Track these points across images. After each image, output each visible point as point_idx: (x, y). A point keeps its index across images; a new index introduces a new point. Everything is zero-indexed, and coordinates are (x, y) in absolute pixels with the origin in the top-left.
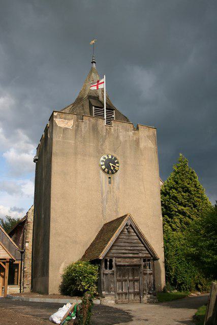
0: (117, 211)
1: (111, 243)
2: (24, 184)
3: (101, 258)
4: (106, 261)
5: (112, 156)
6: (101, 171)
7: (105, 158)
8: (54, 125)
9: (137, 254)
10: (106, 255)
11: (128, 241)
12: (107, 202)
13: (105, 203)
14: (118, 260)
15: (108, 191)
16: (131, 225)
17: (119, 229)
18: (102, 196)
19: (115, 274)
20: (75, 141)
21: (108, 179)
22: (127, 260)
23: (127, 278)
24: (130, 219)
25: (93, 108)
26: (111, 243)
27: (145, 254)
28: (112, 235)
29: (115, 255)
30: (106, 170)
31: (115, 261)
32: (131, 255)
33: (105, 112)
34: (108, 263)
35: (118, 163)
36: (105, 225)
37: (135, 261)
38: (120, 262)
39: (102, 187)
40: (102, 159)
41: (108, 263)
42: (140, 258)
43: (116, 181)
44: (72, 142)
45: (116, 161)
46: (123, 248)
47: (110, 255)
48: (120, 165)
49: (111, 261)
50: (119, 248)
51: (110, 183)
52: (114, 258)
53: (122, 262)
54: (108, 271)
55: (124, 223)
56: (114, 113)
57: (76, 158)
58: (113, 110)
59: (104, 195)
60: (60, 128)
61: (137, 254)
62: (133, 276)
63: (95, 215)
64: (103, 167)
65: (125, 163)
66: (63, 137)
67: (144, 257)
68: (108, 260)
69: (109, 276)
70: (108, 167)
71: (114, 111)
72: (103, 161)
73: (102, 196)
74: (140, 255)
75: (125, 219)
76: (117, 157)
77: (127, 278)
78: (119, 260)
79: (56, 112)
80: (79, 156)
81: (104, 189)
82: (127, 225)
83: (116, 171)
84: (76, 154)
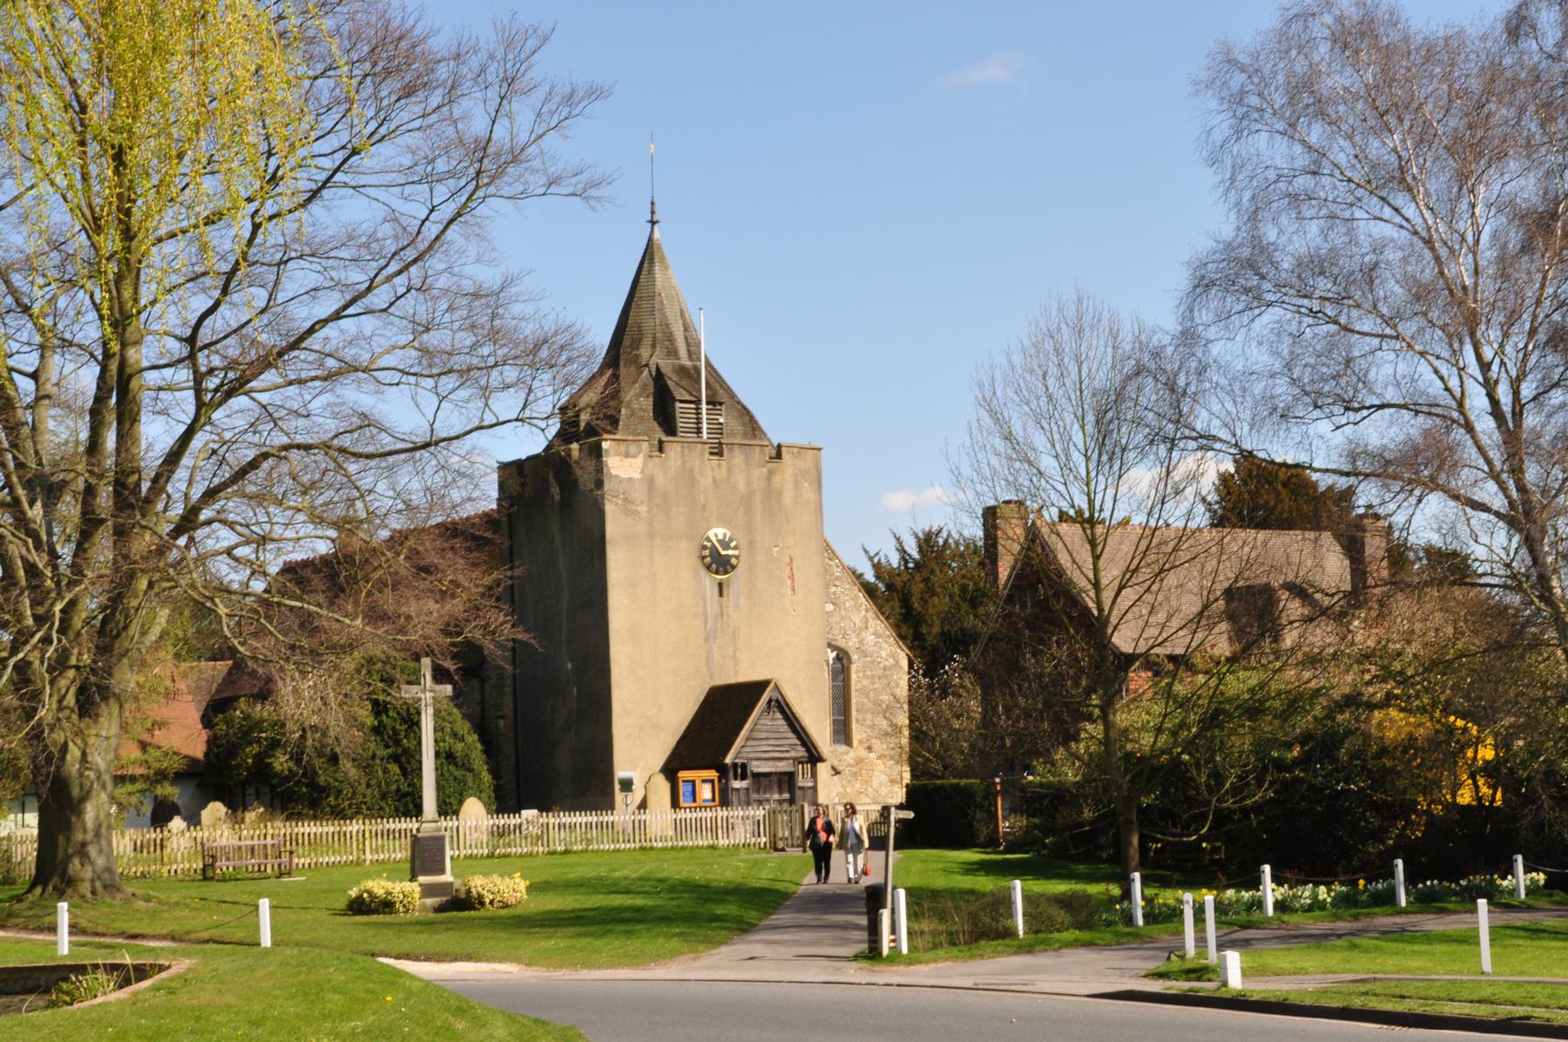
12: (715, 637)
14: (754, 763)
16: (777, 701)
22: (770, 763)
25: (678, 405)
33: (704, 411)
39: (705, 607)
46: (764, 742)
49: (744, 766)
51: (721, 594)
59: (710, 623)
74: (793, 754)
80: (658, 541)
82: (770, 701)
83: (734, 567)
84: (651, 536)
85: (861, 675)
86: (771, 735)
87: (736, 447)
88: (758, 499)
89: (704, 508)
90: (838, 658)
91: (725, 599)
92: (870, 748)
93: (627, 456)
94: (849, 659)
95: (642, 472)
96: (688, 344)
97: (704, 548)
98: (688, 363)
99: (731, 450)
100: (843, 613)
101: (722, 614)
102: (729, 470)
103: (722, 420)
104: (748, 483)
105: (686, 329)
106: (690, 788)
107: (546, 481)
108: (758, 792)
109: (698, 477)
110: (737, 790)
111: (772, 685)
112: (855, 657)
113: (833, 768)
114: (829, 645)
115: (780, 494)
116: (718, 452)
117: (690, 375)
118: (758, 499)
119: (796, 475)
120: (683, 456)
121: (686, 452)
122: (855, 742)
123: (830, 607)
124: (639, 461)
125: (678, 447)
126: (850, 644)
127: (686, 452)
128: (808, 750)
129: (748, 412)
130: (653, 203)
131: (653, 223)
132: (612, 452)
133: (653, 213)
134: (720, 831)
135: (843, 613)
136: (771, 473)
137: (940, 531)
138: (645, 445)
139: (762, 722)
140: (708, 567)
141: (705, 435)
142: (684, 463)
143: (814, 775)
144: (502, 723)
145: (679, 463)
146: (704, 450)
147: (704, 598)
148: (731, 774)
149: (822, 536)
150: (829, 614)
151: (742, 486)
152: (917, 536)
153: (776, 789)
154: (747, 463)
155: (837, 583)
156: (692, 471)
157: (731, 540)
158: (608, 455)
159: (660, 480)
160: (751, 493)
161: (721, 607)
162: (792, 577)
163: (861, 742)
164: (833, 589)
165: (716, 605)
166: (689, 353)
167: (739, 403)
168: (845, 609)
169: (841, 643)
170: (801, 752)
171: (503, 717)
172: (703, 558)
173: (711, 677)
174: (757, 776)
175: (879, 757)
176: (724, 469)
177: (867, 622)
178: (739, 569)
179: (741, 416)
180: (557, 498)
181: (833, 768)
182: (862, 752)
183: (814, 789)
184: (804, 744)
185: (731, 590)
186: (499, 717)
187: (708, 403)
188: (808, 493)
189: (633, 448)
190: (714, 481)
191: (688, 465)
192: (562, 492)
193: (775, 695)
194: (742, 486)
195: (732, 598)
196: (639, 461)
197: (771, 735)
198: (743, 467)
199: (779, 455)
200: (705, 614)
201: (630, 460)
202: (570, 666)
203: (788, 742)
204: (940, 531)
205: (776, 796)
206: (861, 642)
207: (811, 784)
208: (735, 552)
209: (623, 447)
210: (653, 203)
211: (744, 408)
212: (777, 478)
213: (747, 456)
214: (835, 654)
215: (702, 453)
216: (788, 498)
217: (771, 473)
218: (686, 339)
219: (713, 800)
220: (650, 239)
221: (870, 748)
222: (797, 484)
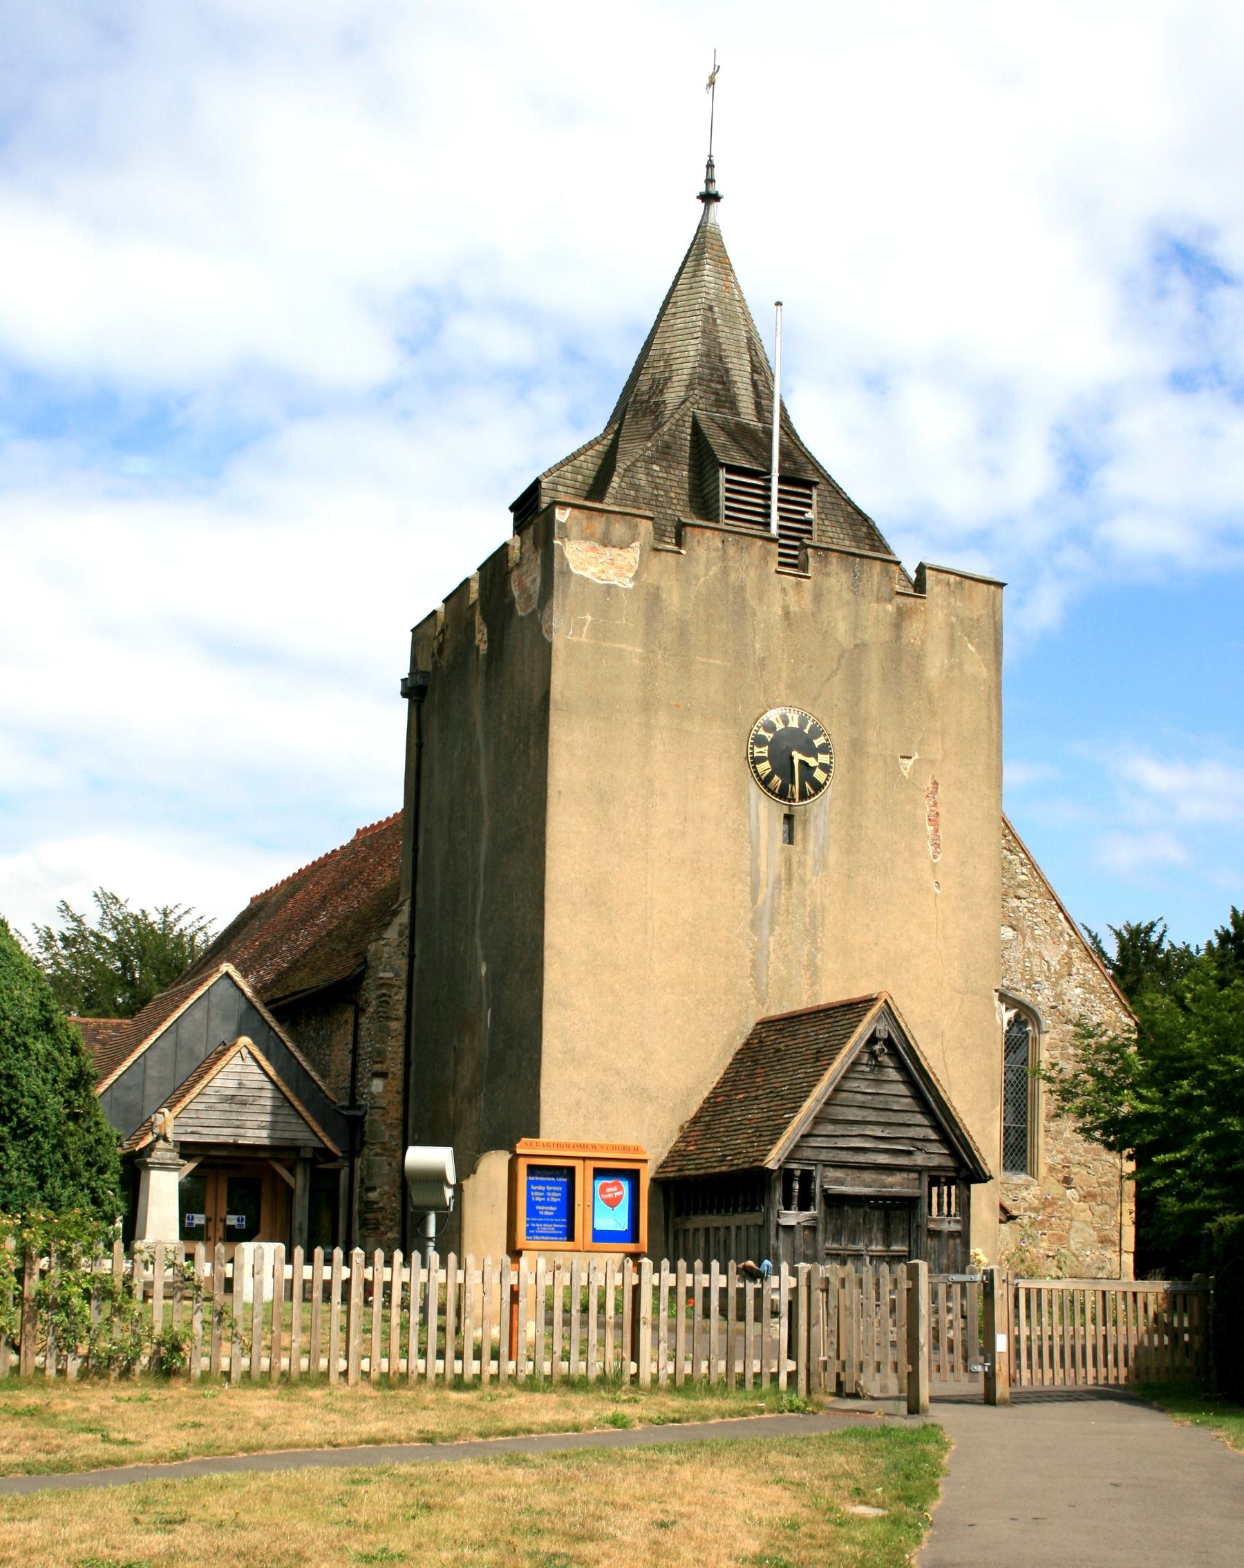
0: (815, 965)
1: (810, 1105)
2: (369, 1236)
3: (772, 1161)
4: (787, 1175)
5: (803, 722)
6: (754, 789)
7: (785, 720)
8: (556, 566)
9: (909, 1153)
10: (790, 1158)
11: (878, 1102)
12: (772, 923)
13: (766, 931)
14: (832, 1173)
15: (779, 878)
16: (889, 1042)
17: (844, 1051)
18: (754, 900)
19: (821, 1227)
20: (645, 646)
21: (780, 827)
22: (868, 1176)
23: (861, 1246)
24: (889, 1012)
25: (723, 474)
26: (810, 1105)
27: (936, 1156)
28: (818, 1076)
29: (824, 1156)
30: (777, 781)
31: (823, 1177)
32: (883, 1159)
33: (775, 494)
34: (796, 1186)
35: (825, 749)
36: (766, 1024)
37: (897, 1185)
38: (840, 1182)
39: (755, 859)
40: (773, 715)
41: (796, 1186)
42: (919, 1170)
43: (812, 832)
44: (633, 650)
45: (818, 742)
46: (856, 1130)
47: (807, 1153)
48: (839, 763)
49: (807, 1178)
50: (839, 1130)
51: (790, 839)
52: (820, 1167)
53: (852, 1186)
54: (792, 1217)
55: (863, 1030)
56: (814, 501)
57: (647, 725)
58: (809, 485)
59: (764, 892)
60: (584, 581)
61: (909, 1153)
62: (887, 1243)
63: (723, 980)
64: (765, 767)
65: (857, 747)
66: (598, 630)
67: (929, 1168)
68: (798, 1173)
69: (800, 1236)
70: (783, 766)
71: (814, 493)
72: (769, 727)
73: (754, 900)
74: (919, 1159)
75: (870, 1015)
76: (825, 724)
77: (861, 1246)
78: (839, 1174)
79: (565, 505)
80: (662, 718)
81: (763, 868)
82: (873, 1040)
83: (818, 787)
84: (647, 706)
85: (1057, 1053)
86: (872, 1116)
87: (834, 558)
88: (874, 662)
89: (762, 663)
90: (1016, 1023)
91: (798, 846)
92: (1067, 1181)
93: (606, 542)
94: (1037, 1021)
95: (637, 577)
96: (757, 394)
97: (759, 741)
98: (757, 425)
99: (824, 561)
100: (1030, 945)
101: (789, 880)
102: (818, 598)
103: (810, 515)
104: (856, 627)
105: (756, 368)
106: (556, 1193)
107: (471, 624)
108: (836, 1237)
109: (753, 603)
110: (790, 1228)
111: (880, 1003)
112: (1047, 1022)
113: (1003, 1209)
114: (1003, 997)
115: (919, 658)
116: (795, 563)
117: (756, 442)
118: (874, 662)
119: (951, 626)
120: (724, 558)
121: (731, 551)
122: (1043, 1170)
123: (1008, 933)
124: (631, 556)
125: (714, 540)
126: (1041, 1000)
127: (731, 551)
128: (954, 1154)
129: (865, 519)
130: (710, 166)
131: (709, 198)
132: (574, 531)
133: (710, 181)
134: (646, 1333)
135: (1030, 945)
136: (902, 615)
137: (1153, 925)
138: (646, 527)
139: (853, 1085)
140: (765, 782)
141: (774, 531)
142: (725, 571)
143: (965, 1206)
144: (377, 1085)
145: (715, 570)
146: (768, 552)
147: (754, 842)
148: (778, 1194)
149: (1000, 809)
150: (1007, 945)
151: (842, 628)
152: (1119, 935)
153: (877, 1234)
154: (855, 588)
155: (1021, 892)
156: (742, 589)
157: (816, 732)
158: (565, 536)
159: (673, 598)
160: (861, 647)
161: (788, 862)
162: (934, 819)
163: (1052, 1169)
164: (1016, 902)
165: (778, 858)
166: (758, 406)
167: (849, 502)
168: (1033, 938)
169: (1025, 996)
170: (936, 1156)
171: (383, 1075)
172: (757, 760)
173: (761, 1001)
174: (835, 1202)
175: (1088, 1197)
176: (808, 597)
177: (1070, 964)
178: (828, 793)
179: (853, 524)
180: (483, 648)
181: (1003, 1209)
182: (1056, 1189)
183: (963, 1237)
184: (945, 1140)
185: (812, 832)
186: (377, 1075)
187: (782, 480)
188: (975, 664)
189: (619, 529)
190: (787, 614)
191: (733, 577)
192: (491, 641)
193: (883, 1029)
194: (842, 628)
195: (811, 846)
196: (631, 556)
197: (872, 1116)
198: (847, 596)
199: (920, 586)
200: (754, 873)
201: (610, 552)
202: (483, 970)
203: (911, 1132)
204: (1153, 925)
205: (877, 1248)
206: (1059, 996)
207: (958, 1227)
208: (823, 759)
209: (599, 524)
210: (710, 166)
211: (859, 512)
212: (914, 629)
213: (856, 580)
214: (1011, 1014)
215: (765, 558)
216: (936, 665)
217: (902, 615)
218: (754, 384)
219: (633, 1234)
220: (702, 227)
221: (1067, 1181)
222: (952, 643)
